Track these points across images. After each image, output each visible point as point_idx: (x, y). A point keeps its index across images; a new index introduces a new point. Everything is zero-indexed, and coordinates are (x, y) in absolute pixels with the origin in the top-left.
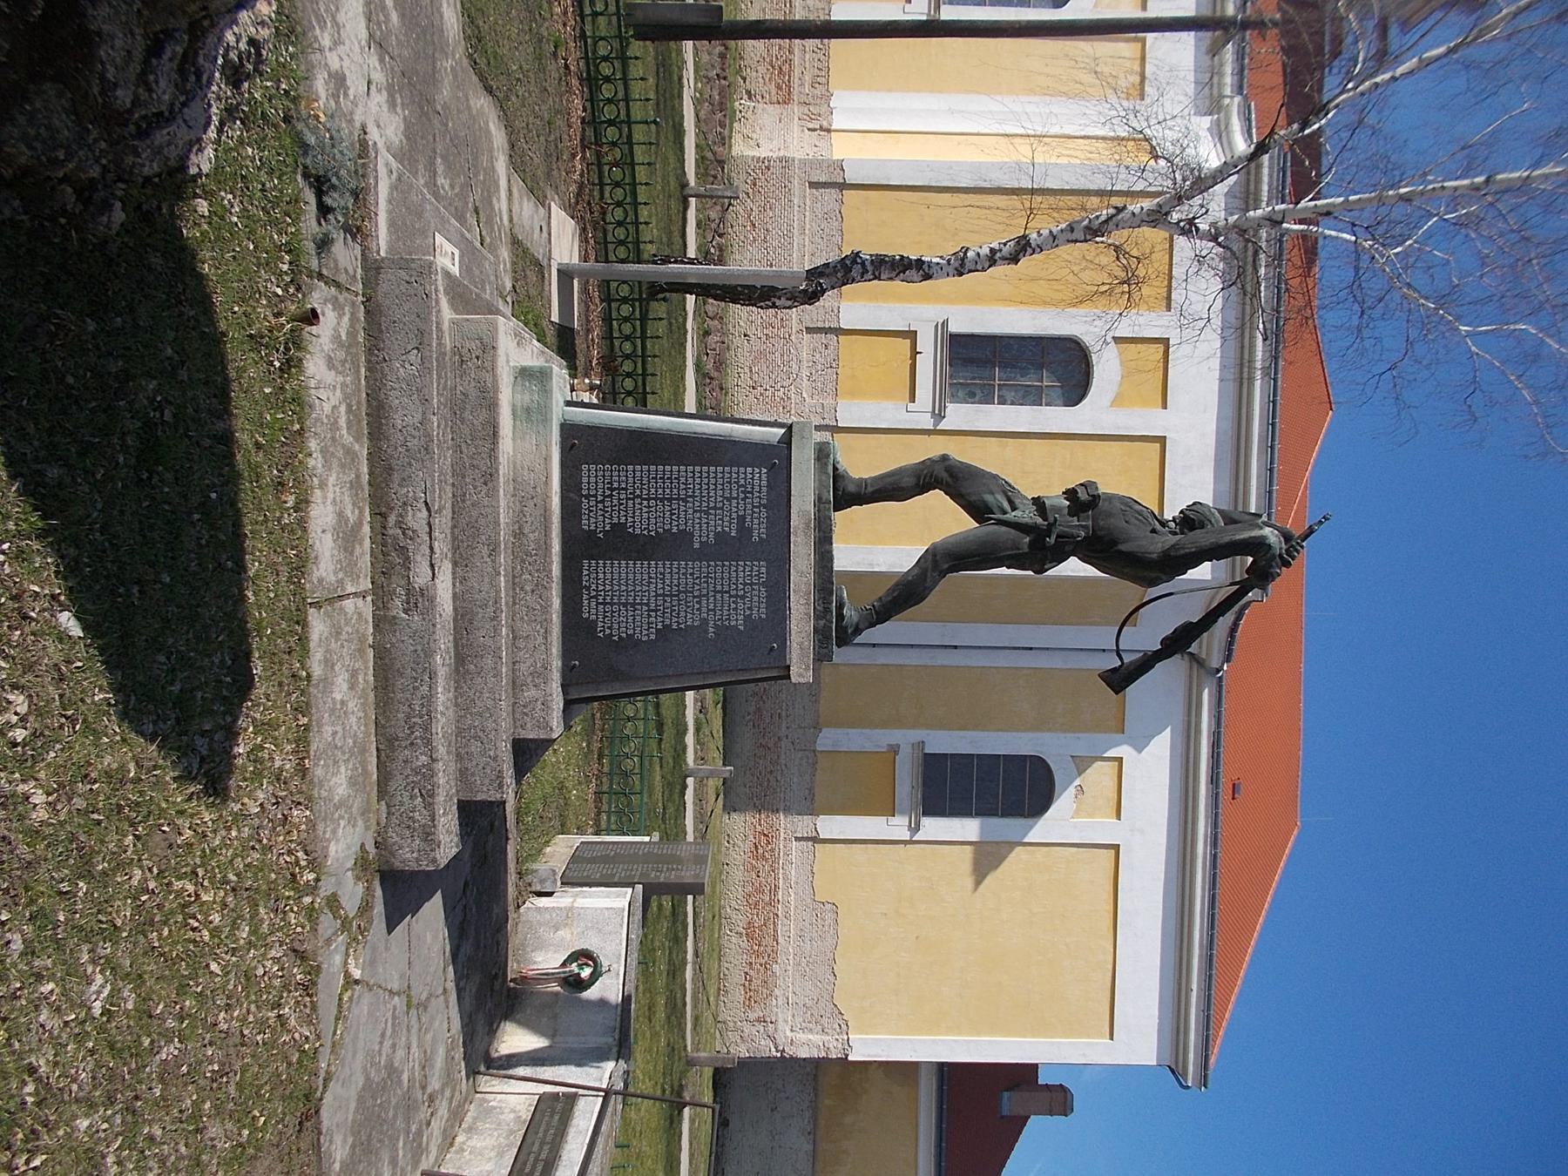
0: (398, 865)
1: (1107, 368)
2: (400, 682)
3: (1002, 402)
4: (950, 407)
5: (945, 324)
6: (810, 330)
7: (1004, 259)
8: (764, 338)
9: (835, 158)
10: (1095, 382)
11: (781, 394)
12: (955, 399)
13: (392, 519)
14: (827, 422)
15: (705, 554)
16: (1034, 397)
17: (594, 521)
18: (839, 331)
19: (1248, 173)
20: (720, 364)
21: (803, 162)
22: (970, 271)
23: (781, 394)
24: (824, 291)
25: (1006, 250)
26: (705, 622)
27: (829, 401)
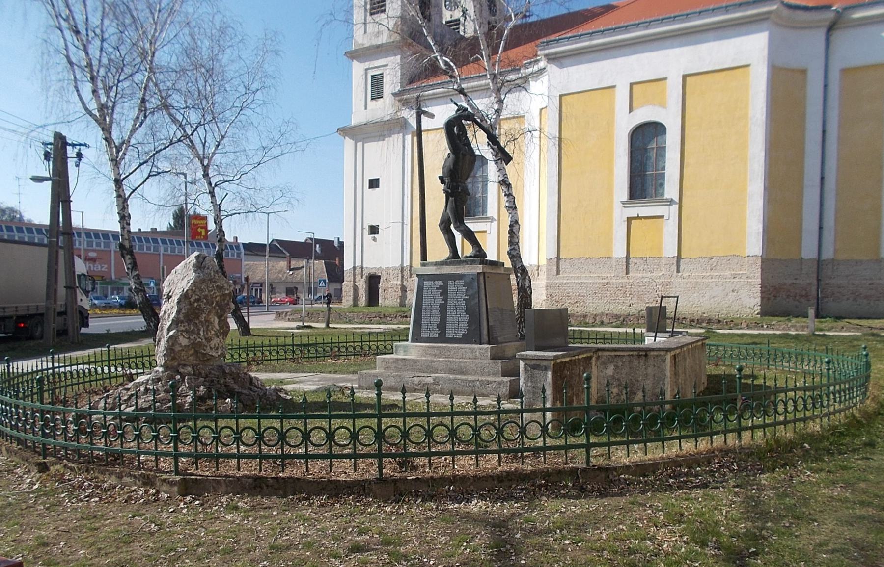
0: (508, 393)
1: (643, 115)
2: (457, 388)
3: (664, 168)
4: (667, 196)
5: (623, 203)
6: (627, 273)
7: (508, 190)
8: (631, 296)
9: (545, 263)
10: (653, 119)
11: (660, 287)
12: (663, 194)
13: (416, 387)
14: (675, 262)
15: (446, 300)
16: (662, 150)
17: (436, 334)
18: (628, 258)
19: (475, 90)
20: (617, 317)
21: (548, 278)
22: (514, 204)
23: (660, 287)
24: (522, 266)
25: (505, 190)
26: (464, 299)
27: (664, 261)
